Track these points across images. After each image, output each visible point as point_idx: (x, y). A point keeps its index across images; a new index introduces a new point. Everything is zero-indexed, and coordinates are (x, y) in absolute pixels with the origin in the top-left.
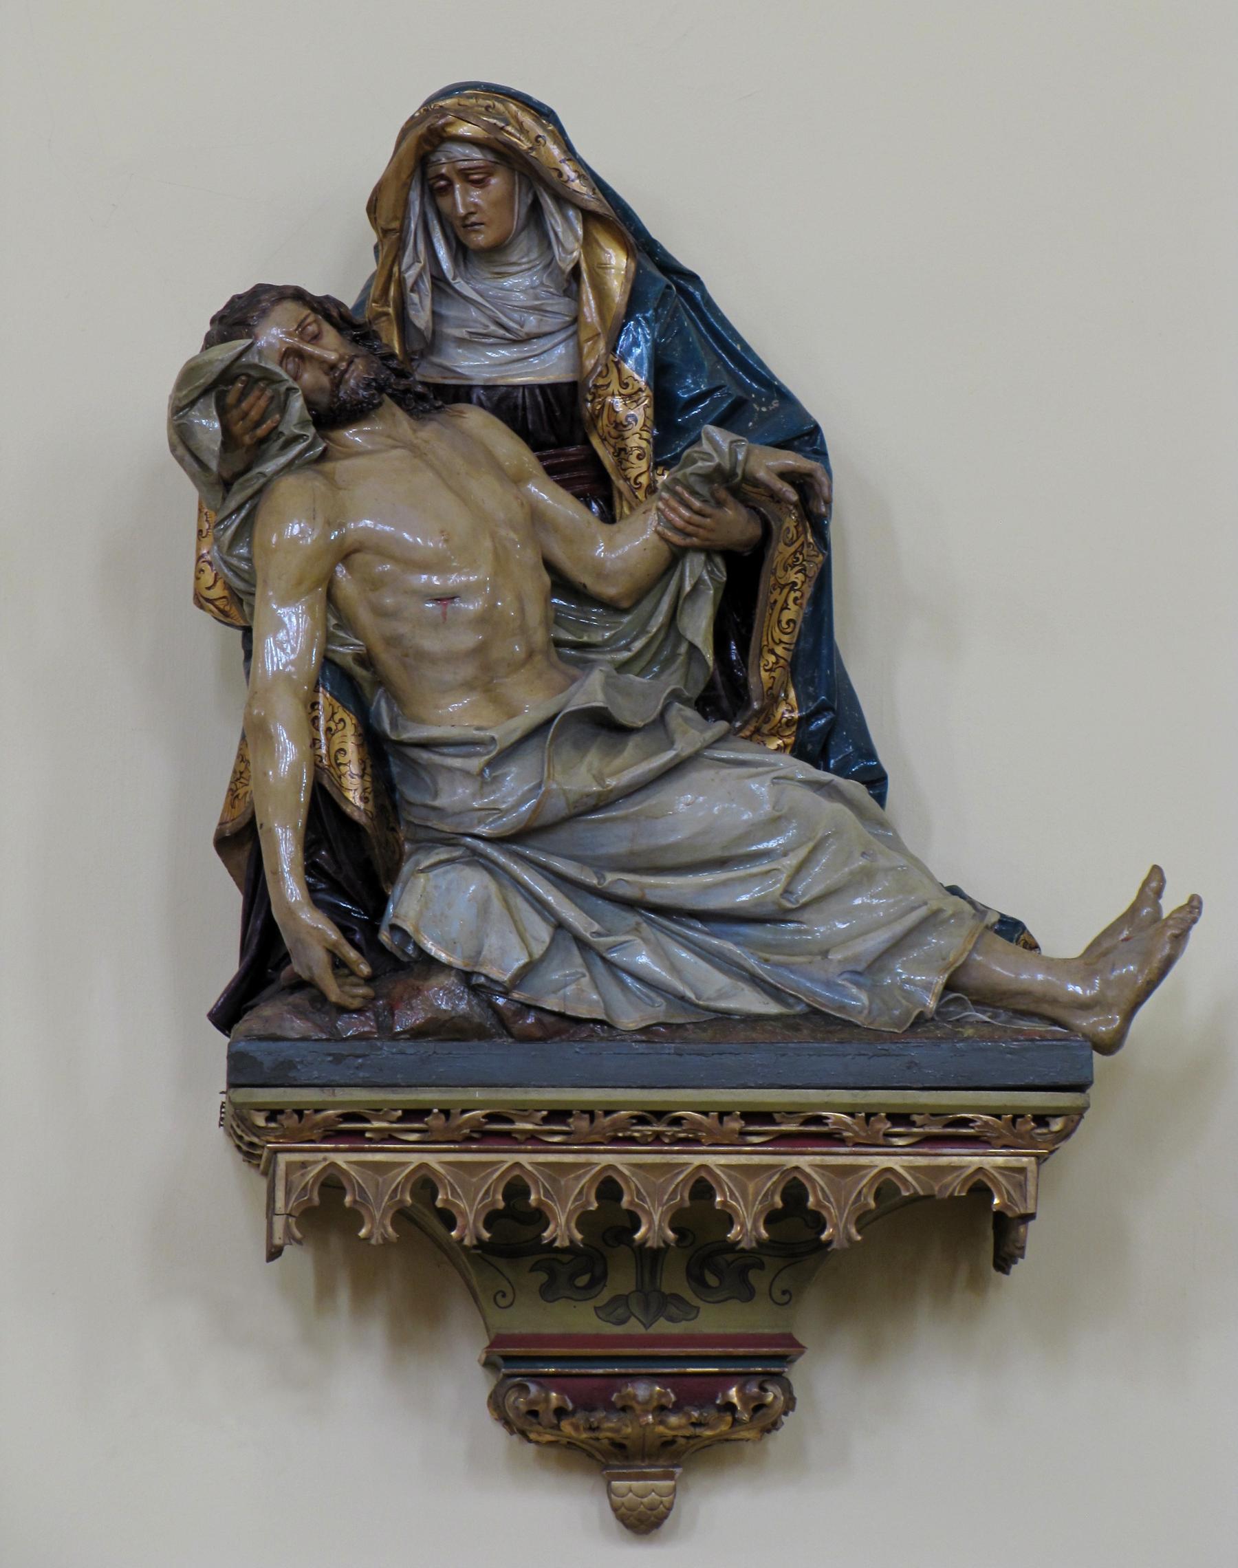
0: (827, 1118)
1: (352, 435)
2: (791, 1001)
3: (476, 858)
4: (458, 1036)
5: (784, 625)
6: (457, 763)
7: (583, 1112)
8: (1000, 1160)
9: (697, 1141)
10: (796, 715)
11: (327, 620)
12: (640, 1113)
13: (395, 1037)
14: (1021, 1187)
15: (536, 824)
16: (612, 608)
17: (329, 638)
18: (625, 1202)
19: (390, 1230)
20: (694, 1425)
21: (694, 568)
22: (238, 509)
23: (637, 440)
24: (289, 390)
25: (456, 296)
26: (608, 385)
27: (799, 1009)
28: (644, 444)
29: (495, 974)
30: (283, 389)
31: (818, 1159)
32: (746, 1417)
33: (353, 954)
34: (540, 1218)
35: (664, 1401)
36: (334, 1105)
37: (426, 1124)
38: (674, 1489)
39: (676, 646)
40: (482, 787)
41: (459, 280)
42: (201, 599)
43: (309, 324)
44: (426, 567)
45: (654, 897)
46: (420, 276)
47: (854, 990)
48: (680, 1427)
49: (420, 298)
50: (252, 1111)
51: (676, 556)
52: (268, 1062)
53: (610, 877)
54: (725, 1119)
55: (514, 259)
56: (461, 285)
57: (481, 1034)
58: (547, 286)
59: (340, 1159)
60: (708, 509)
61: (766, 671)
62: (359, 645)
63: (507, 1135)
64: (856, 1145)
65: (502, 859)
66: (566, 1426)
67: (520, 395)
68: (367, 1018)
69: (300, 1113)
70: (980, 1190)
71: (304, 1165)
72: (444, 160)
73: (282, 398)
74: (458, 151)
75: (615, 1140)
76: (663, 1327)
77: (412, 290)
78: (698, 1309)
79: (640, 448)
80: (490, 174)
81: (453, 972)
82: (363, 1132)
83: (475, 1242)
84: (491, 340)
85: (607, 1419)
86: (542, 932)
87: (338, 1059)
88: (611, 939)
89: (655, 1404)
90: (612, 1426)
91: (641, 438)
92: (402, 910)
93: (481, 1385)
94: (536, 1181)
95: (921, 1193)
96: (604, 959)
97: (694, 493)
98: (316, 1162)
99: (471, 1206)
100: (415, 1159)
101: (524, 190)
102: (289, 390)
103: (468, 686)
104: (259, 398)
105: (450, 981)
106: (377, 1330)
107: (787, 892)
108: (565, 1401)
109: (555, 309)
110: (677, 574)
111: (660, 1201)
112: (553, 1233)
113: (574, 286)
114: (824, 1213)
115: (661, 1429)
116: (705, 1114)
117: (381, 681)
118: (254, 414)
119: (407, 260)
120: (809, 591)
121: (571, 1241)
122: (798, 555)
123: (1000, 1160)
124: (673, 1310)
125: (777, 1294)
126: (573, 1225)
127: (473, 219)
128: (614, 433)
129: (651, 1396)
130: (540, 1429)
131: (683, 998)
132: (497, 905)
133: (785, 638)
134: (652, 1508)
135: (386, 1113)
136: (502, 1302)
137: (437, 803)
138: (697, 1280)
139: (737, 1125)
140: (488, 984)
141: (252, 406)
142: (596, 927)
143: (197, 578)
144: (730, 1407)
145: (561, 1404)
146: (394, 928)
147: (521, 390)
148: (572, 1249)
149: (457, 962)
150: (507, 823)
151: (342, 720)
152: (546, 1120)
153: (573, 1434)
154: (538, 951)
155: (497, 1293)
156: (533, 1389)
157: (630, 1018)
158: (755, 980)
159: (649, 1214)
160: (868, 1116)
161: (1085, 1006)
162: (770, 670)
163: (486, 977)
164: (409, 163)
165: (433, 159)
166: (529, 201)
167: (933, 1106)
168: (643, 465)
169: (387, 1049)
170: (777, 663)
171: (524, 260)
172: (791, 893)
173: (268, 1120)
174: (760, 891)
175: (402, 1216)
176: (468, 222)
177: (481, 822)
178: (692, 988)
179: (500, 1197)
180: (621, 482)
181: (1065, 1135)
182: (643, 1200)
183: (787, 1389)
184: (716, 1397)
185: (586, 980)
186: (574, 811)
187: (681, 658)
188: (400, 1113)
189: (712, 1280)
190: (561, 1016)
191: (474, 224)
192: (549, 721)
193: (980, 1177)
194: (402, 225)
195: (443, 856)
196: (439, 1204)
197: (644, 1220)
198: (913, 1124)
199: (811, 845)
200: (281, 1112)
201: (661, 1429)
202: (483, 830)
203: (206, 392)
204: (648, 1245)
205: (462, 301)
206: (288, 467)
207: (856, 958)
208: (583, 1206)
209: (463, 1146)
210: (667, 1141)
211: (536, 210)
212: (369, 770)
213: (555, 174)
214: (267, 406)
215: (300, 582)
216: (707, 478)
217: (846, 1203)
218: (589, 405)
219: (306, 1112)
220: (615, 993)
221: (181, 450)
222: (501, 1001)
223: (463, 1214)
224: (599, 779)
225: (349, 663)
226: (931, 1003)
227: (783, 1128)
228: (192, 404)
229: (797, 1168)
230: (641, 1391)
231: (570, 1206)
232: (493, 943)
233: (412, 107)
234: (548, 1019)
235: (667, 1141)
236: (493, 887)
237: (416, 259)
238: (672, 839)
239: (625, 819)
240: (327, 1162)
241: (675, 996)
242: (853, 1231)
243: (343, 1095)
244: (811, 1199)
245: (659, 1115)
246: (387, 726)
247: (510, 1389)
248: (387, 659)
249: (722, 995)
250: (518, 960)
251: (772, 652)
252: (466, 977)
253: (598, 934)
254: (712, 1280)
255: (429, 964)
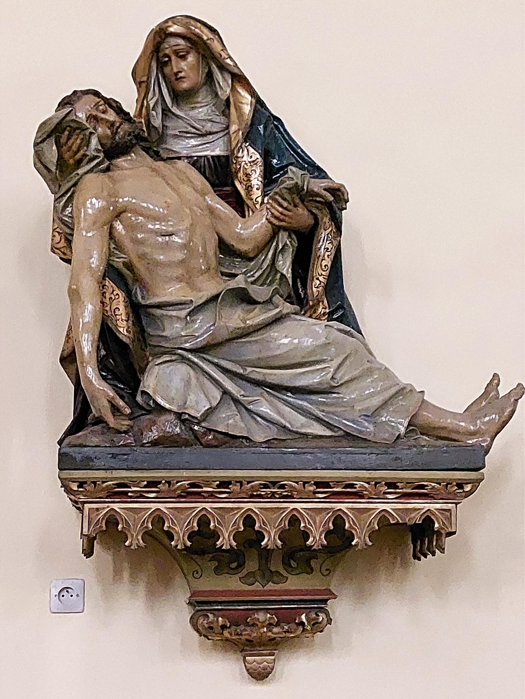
0: (356, 484)
1: (120, 161)
2: (336, 429)
3: (184, 361)
4: (175, 445)
5: (323, 267)
6: (174, 313)
7: (237, 482)
8: (438, 506)
9: (292, 497)
10: (328, 311)
11: (109, 244)
12: (265, 482)
13: (143, 445)
14: (449, 519)
15: (213, 342)
16: (246, 257)
17: (110, 254)
18: (257, 527)
19: (141, 541)
20: (285, 632)
21: (283, 237)
22: (66, 192)
23: (256, 180)
24: (91, 133)
25: (173, 117)
26: (243, 157)
27: (340, 433)
28: (260, 183)
29: (193, 413)
30: (87, 133)
31: (350, 505)
32: (309, 628)
33: (121, 403)
34: (215, 535)
35: (272, 621)
36: (112, 479)
37: (159, 488)
38: (274, 660)
39: (276, 274)
40: (186, 325)
41: (174, 107)
42: (54, 249)
43: (101, 105)
44: (156, 219)
45: (269, 380)
46: (156, 103)
47: (366, 424)
48: (279, 633)
49: (156, 113)
50: (70, 482)
51: (276, 231)
52: (79, 457)
53: (249, 369)
54: (306, 485)
55: (199, 100)
56: (175, 110)
57: (187, 444)
58: (215, 112)
59: (116, 506)
60: (291, 207)
61: (315, 287)
62: (125, 258)
63: (199, 494)
64: (369, 498)
65: (196, 360)
66: (226, 633)
67: (203, 160)
68: (129, 436)
69: (95, 483)
70: (428, 521)
71: (98, 509)
72: (167, 46)
73: (87, 137)
74: (173, 41)
75: (252, 496)
76: (270, 586)
77: (152, 110)
78: (287, 578)
79: (257, 185)
80: (188, 53)
81: (172, 413)
82: (126, 493)
83: (183, 547)
84: (189, 135)
85: (245, 630)
86: (217, 394)
87: (114, 456)
88: (250, 399)
89: (268, 622)
90: (248, 633)
91: (258, 180)
92: (146, 384)
93: (187, 613)
94: (213, 516)
95: (401, 522)
96: (246, 409)
97: (285, 199)
98: (104, 508)
99: (181, 530)
100: (154, 506)
101: (204, 66)
102: (91, 133)
103: (179, 279)
104: (77, 139)
105: (172, 417)
106: (141, 590)
107: (333, 378)
108: (226, 622)
109: (218, 121)
110: (276, 239)
111: (274, 527)
112: (221, 542)
113: (227, 111)
114: (354, 532)
115: (270, 634)
116: (297, 483)
117: (137, 279)
118: (74, 148)
119: (150, 95)
120: (333, 252)
121: (231, 546)
122: (329, 235)
123: (438, 506)
124: (275, 579)
125: (323, 569)
126: (231, 538)
127: (181, 75)
128: (246, 179)
129: (266, 619)
130: (214, 635)
131: (285, 427)
132: (194, 381)
133: (324, 273)
134: (264, 669)
135: (139, 483)
136: (195, 575)
137: (164, 334)
138: (287, 565)
139: (312, 488)
140: (190, 418)
141: (73, 144)
142: (242, 393)
143: (52, 240)
144: (302, 624)
145: (224, 623)
146: (144, 393)
147: (203, 158)
148: (231, 550)
149: (174, 408)
150: (200, 342)
151: (117, 294)
152: (218, 486)
153: (229, 636)
154: (214, 404)
155: (193, 574)
156: (211, 616)
157: (259, 437)
158: (318, 420)
159: (269, 533)
160: (376, 483)
161: (473, 434)
162: (317, 287)
163: (189, 415)
164: (151, 48)
165: (162, 47)
166: (206, 71)
167: (407, 479)
168: (259, 193)
169: (139, 449)
170: (320, 284)
171: (204, 101)
172: (335, 379)
173: (79, 487)
174: (319, 378)
175: (147, 534)
176: (178, 77)
177: (186, 342)
178: (290, 423)
179: (195, 524)
180: (249, 201)
181: (471, 493)
182: (266, 525)
183: (327, 614)
184: (295, 620)
185: (238, 417)
186: (231, 337)
187: (277, 281)
188: (145, 483)
189: (293, 564)
190: (226, 434)
191: (181, 78)
192: (217, 296)
193: (428, 514)
194: (148, 79)
195: (168, 359)
196: (165, 528)
197: (266, 535)
198: (397, 487)
199: (344, 356)
200: (85, 483)
201: (270, 634)
202: (187, 345)
203: (49, 136)
204: (269, 548)
205: (176, 118)
206: (91, 171)
207: (367, 409)
208: (237, 529)
209: (178, 500)
210: (278, 496)
211: (210, 75)
212: (131, 319)
213: (219, 56)
214: (81, 143)
215: (94, 223)
216: (290, 190)
217: (364, 528)
218: (234, 165)
219: (98, 483)
220: (252, 423)
221: (39, 165)
222: (196, 428)
223: (177, 533)
224: (244, 321)
225: (121, 266)
226: (403, 430)
227: (335, 489)
228: (43, 141)
229: (340, 510)
230: (261, 616)
231: (230, 529)
232: (192, 398)
233: (153, 25)
234: (220, 436)
235: (278, 496)
236: (192, 372)
237: (154, 95)
238: (278, 352)
239: (256, 341)
240: (109, 509)
241: (281, 427)
242: (367, 539)
243: (116, 474)
244: (347, 525)
245: (274, 484)
246: (140, 300)
247: (200, 616)
248: (140, 266)
249: (303, 426)
250: (205, 406)
251: (318, 279)
252: (179, 415)
253: (244, 396)
254: (293, 564)
255: (160, 409)
